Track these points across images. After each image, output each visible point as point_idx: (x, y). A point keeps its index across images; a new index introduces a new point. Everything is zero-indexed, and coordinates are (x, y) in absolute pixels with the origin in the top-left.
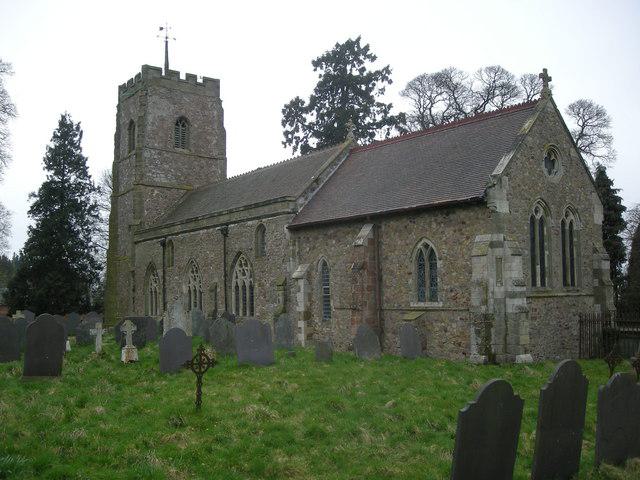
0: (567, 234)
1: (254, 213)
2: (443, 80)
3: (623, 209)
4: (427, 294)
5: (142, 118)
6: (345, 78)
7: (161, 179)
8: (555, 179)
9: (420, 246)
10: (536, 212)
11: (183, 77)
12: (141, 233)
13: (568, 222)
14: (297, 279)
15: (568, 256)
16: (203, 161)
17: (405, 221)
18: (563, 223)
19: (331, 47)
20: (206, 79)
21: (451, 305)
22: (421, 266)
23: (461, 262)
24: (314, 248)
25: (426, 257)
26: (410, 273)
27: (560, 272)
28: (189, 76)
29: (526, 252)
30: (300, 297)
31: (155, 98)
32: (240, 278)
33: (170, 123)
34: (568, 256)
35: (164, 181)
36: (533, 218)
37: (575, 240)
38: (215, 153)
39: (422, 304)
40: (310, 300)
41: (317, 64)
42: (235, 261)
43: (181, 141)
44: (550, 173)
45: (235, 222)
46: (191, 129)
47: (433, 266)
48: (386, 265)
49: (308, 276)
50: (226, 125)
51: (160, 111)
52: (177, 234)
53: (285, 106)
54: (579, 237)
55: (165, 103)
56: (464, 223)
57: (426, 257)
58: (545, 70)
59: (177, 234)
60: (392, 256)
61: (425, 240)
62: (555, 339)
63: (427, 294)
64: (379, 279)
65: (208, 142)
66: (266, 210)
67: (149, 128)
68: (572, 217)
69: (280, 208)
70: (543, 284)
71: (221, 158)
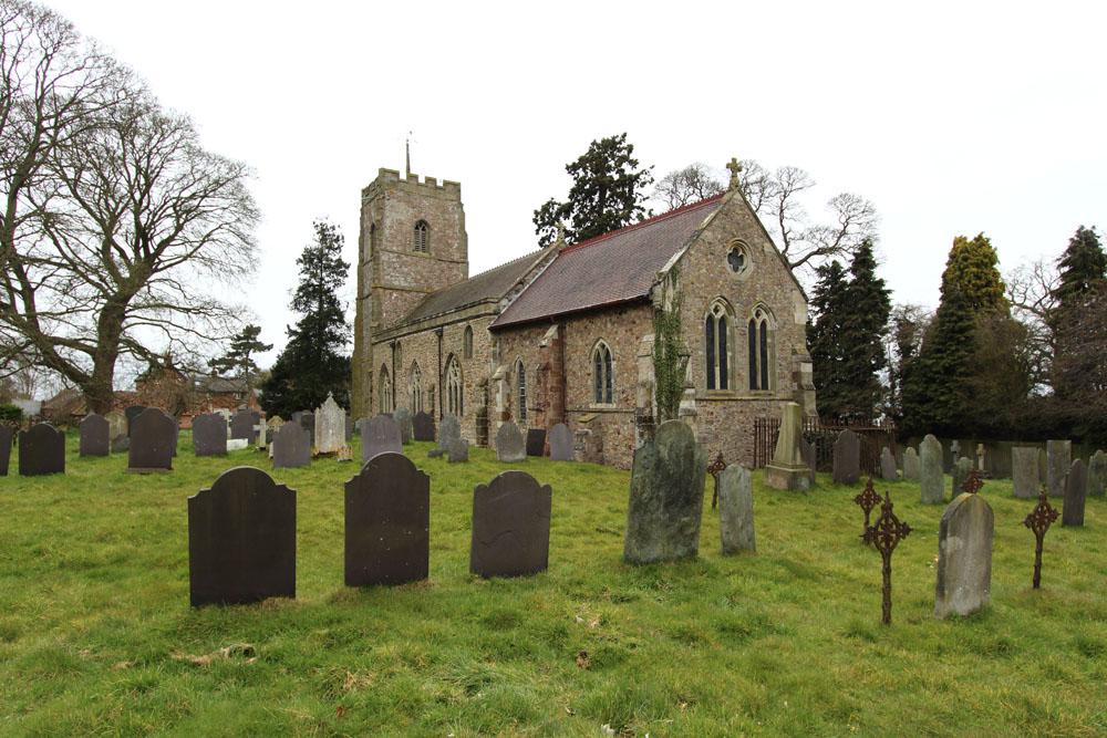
0: (758, 338)
1: (464, 315)
2: (692, 177)
3: (890, 308)
4: (604, 396)
5: (380, 222)
6: (603, 177)
7: (400, 282)
8: (743, 276)
9: (597, 346)
10: (716, 310)
11: (422, 180)
12: (381, 334)
13: (758, 322)
14: (496, 380)
15: (759, 356)
16: (443, 265)
17: (586, 322)
18: (752, 322)
19: (584, 151)
20: (446, 183)
21: (623, 406)
22: (599, 368)
23: (630, 364)
24: (512, 349)
25: (602, 357)
26: (589, 375)
27: (746, 374)
28: (428, 180)
29: (701, 353)
30: (499, 397)
31: (393, 202)
32: (452, 379)
33: (409, 227)
34: (759, 356)
35: (403, 284)
36: (710, 318)
37: (769, 340)
38: (456, 257)
39: (599, 406)
40: (509, 400)
41: (572, 169)
42: (448, 362)
43: (423, 246)
44: (736, 270)
45: (448, 324)
46: (432, 233)
47: (609, 367)
48: (569, 366)
49: (508, 377)
50: (468, 229)
51: (398, 215)
52: (404, 335)
53: (536, 213)
54: (773, 337)
55: (403, 206)
56: (634, 323)
57: (602, 357)
58: (734, 160)
59: (404, 335)
60: (574, 356)
61: (601, 341)
62: (739, 444)
63: (604, 396)
64: (563, 381)
65: (450, 245)
66: (472, 312)
67: (387, 232)
68: (764, 316)
69: (482, 309)
70: (724, 385)
71: (464, 262)
